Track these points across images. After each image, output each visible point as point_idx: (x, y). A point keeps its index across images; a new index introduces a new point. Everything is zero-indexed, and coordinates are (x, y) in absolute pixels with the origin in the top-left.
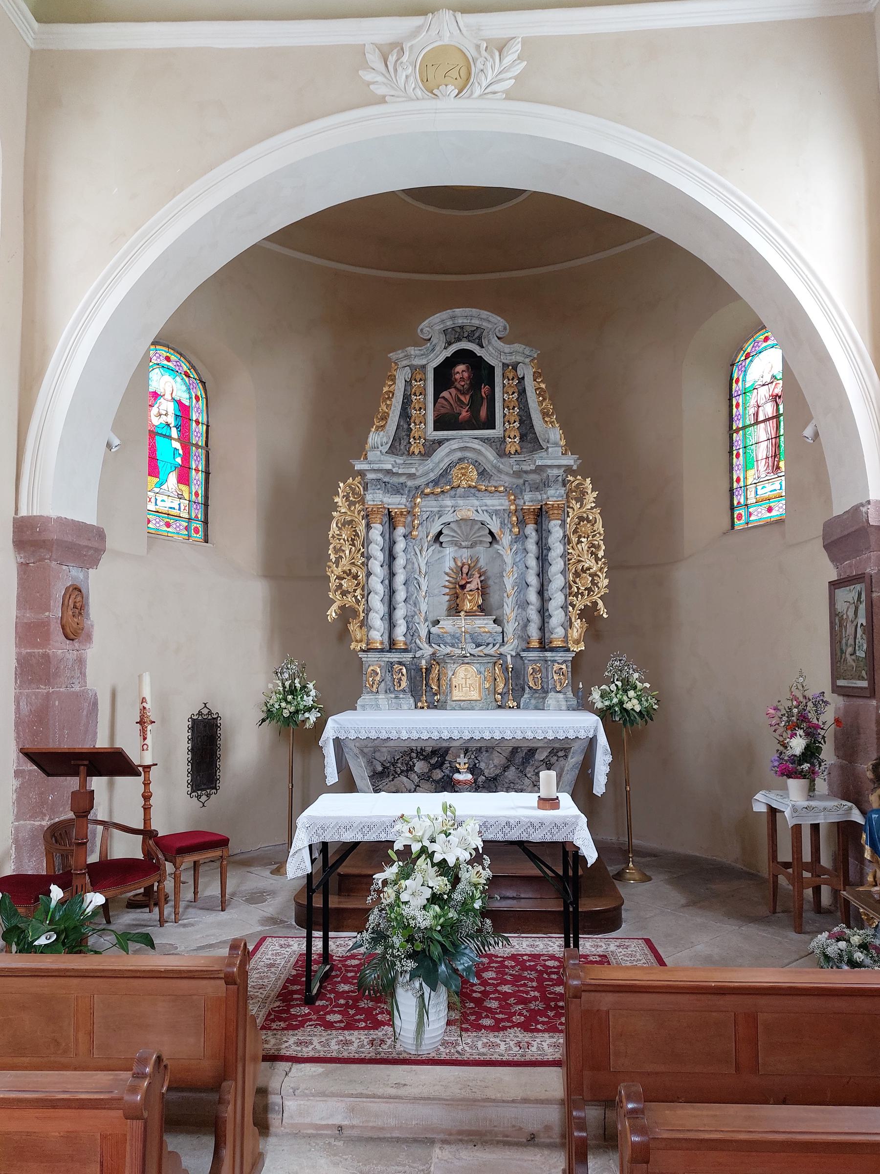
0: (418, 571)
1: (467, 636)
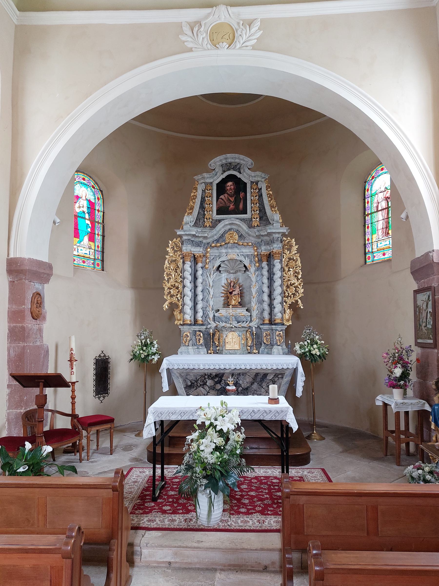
0: (209, 285)
1: (233, 317)
